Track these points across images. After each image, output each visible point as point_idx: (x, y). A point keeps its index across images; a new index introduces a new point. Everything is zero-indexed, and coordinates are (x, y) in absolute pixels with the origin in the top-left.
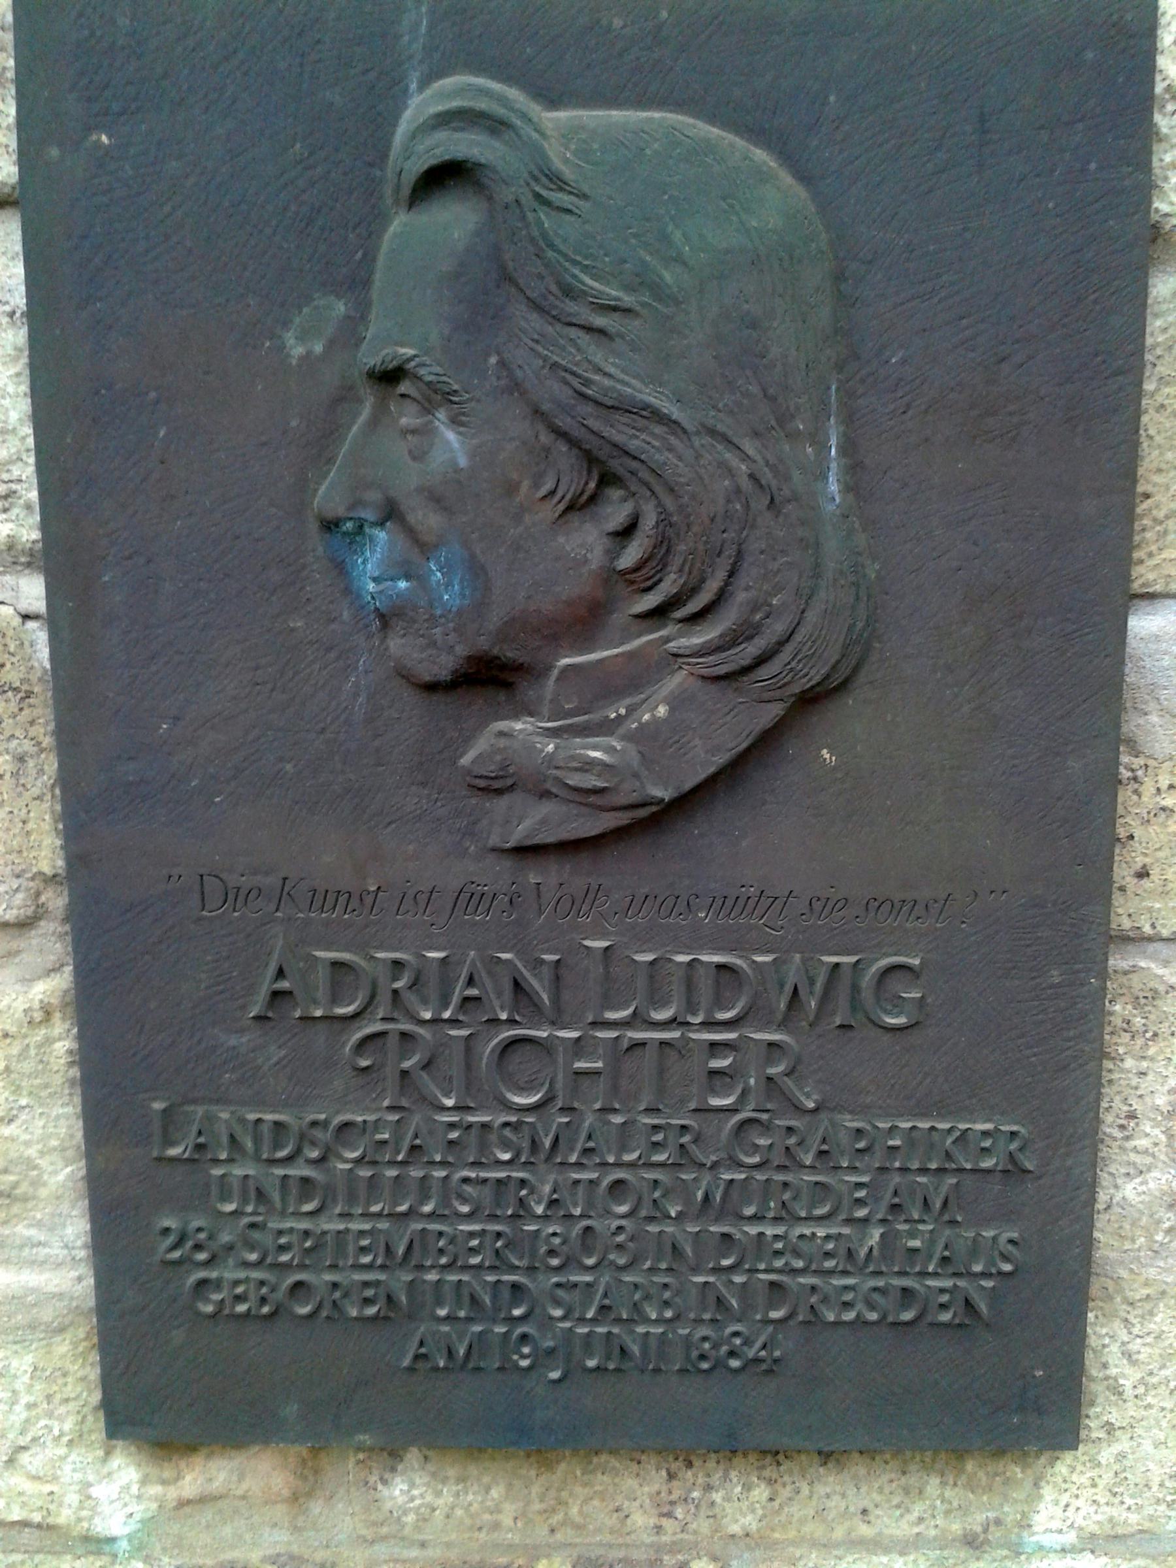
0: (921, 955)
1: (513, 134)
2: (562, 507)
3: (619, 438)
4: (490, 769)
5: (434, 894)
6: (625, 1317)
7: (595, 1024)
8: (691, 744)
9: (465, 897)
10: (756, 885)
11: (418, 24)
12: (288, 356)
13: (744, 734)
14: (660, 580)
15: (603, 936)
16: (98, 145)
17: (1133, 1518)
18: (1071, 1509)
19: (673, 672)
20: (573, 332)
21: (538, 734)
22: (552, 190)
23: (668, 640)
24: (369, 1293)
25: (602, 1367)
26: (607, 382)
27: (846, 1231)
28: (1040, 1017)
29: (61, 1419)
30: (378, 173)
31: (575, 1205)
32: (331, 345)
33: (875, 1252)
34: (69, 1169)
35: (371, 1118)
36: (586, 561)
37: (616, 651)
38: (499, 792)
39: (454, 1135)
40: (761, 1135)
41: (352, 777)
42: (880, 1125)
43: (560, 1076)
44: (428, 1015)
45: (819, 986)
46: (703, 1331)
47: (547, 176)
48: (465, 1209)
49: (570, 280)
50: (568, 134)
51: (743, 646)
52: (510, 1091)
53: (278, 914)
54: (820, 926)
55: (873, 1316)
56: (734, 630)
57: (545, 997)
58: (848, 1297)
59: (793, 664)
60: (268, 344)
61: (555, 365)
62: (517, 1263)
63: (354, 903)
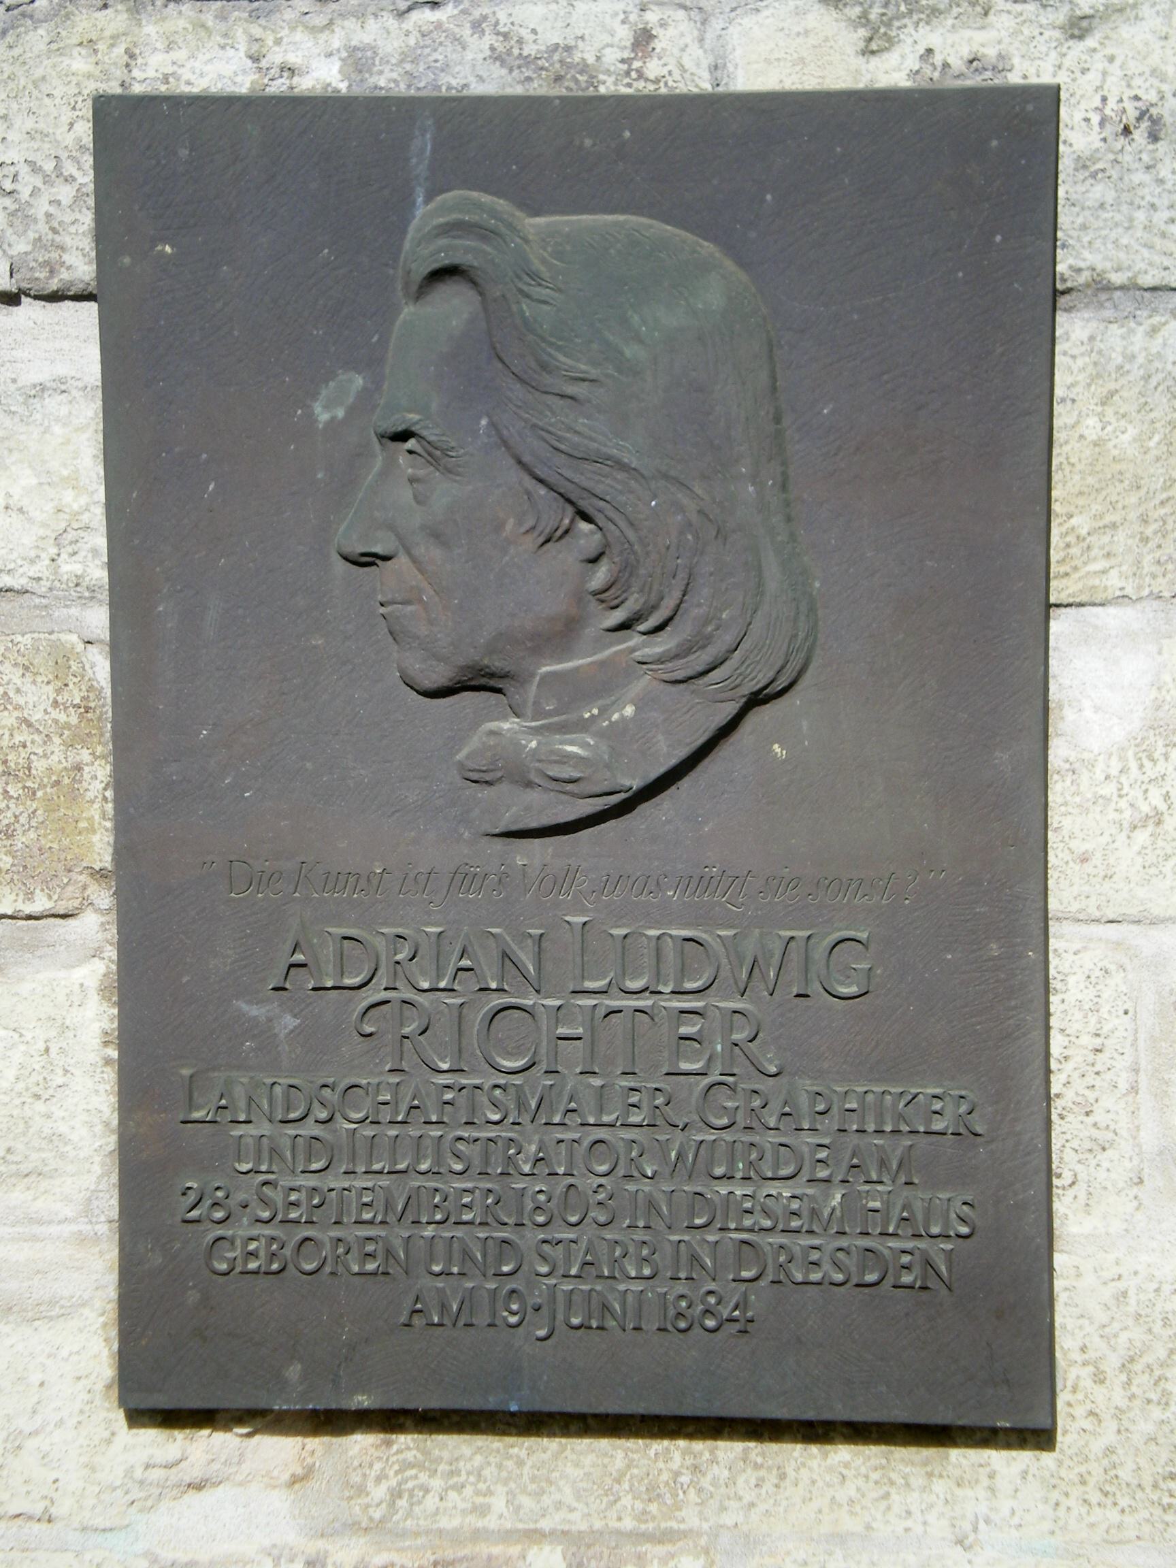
0: (869, 929)
1: (500, 240)
3: (585, 484)
4: (482, 764)
5: (432, 874)
6: (606, 1274)
8: (655, 740)
9: (459, 877)
10: (718, 865)
11: (423, 150)
12: (316, 421)
13: (701, 731)
15: (583, 912)
18: (1062, 1509)
19: (638, 678)
20: (550, 400)
21: (524, 732)
22: (530, 285)
24: (370, 1248)
25: (586, 1324)
26: (576, 439)
27: (810, 1191)
28: (983, 987)
31: (560, 1165)
32: (351, 411)
33: (838, 1213)
35: (375, 1081)
37: (589, 660)
39: (448, 1096)
40: (729, 1098)
41: (362, 772)
42: (838, 1089)
44: (426, 985)
46: (681, 1288)
47: (528, 274)
48: (458, 1167)
49: (546, 358)
51: (698, 654)
52: (499, 1055)
53: (297, 895)
54: (776, 903)
55: (839, 1277)
56: (690, 641)
57: (531, 968)
58: (815, 1256)
59: (743, 668)
60: (299, 412)
61: (534, 426)
62: (506, 1220)
63: (363, 883)
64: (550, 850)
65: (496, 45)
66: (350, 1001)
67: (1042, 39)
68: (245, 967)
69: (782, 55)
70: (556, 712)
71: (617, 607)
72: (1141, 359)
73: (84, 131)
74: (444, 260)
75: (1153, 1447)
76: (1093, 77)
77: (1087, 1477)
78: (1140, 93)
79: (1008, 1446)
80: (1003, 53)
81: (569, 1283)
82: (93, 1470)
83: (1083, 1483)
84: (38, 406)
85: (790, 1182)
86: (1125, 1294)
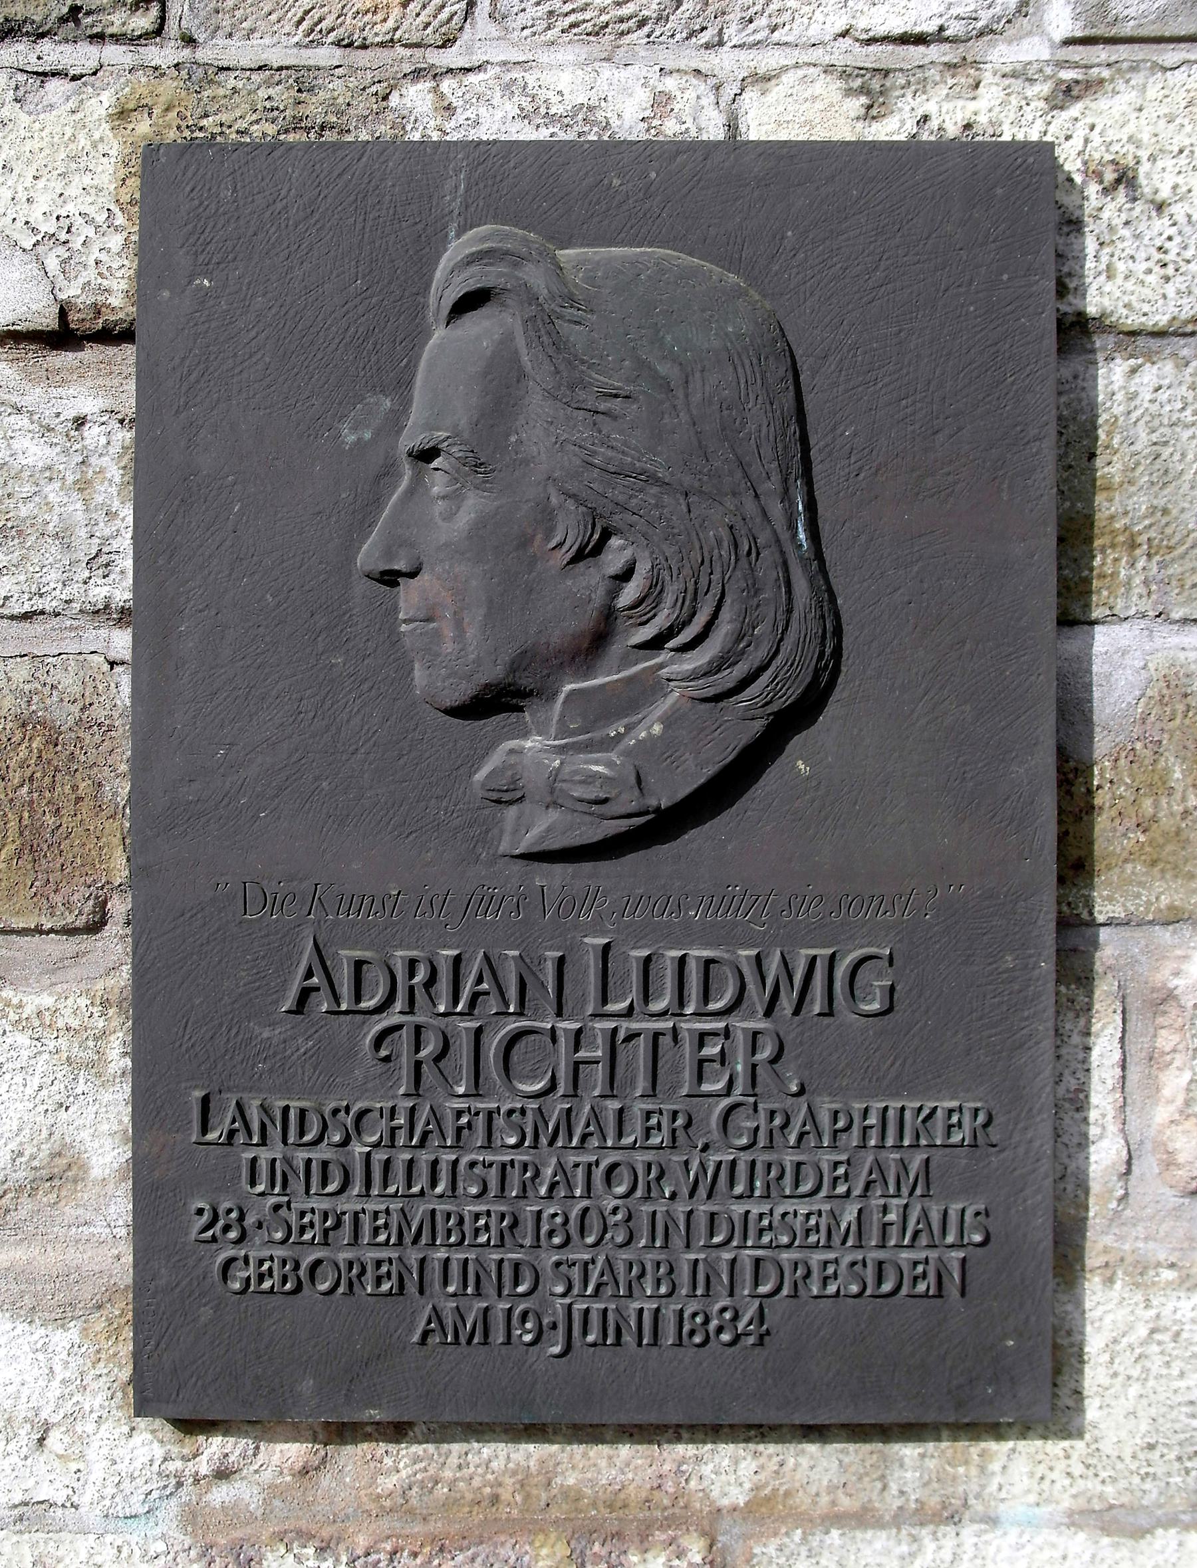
4: (503, 783)
7: (594, 1015)
14: (655, 615)
15: (603, 933)
16: (201, 287)
17: (1109, 1489)
18: (1047, 1482)
23: (661, 666)
29: (94, 1394)
30: (422, 300)
32: (377, 434)
37: (615, 677)
38: (510, 803)
43: (563, 1064)
50: (579, 264)
65: (524, 104)
67: (1028, 109)
68: (258, 988)
69: (791, 117)
74: (473, 285)
75: (1133, 1421)
80: (994, 120)
81: (583, 1302)
82: (114, 1463)
83: (1068, 1457)
84: (1071, 1050)
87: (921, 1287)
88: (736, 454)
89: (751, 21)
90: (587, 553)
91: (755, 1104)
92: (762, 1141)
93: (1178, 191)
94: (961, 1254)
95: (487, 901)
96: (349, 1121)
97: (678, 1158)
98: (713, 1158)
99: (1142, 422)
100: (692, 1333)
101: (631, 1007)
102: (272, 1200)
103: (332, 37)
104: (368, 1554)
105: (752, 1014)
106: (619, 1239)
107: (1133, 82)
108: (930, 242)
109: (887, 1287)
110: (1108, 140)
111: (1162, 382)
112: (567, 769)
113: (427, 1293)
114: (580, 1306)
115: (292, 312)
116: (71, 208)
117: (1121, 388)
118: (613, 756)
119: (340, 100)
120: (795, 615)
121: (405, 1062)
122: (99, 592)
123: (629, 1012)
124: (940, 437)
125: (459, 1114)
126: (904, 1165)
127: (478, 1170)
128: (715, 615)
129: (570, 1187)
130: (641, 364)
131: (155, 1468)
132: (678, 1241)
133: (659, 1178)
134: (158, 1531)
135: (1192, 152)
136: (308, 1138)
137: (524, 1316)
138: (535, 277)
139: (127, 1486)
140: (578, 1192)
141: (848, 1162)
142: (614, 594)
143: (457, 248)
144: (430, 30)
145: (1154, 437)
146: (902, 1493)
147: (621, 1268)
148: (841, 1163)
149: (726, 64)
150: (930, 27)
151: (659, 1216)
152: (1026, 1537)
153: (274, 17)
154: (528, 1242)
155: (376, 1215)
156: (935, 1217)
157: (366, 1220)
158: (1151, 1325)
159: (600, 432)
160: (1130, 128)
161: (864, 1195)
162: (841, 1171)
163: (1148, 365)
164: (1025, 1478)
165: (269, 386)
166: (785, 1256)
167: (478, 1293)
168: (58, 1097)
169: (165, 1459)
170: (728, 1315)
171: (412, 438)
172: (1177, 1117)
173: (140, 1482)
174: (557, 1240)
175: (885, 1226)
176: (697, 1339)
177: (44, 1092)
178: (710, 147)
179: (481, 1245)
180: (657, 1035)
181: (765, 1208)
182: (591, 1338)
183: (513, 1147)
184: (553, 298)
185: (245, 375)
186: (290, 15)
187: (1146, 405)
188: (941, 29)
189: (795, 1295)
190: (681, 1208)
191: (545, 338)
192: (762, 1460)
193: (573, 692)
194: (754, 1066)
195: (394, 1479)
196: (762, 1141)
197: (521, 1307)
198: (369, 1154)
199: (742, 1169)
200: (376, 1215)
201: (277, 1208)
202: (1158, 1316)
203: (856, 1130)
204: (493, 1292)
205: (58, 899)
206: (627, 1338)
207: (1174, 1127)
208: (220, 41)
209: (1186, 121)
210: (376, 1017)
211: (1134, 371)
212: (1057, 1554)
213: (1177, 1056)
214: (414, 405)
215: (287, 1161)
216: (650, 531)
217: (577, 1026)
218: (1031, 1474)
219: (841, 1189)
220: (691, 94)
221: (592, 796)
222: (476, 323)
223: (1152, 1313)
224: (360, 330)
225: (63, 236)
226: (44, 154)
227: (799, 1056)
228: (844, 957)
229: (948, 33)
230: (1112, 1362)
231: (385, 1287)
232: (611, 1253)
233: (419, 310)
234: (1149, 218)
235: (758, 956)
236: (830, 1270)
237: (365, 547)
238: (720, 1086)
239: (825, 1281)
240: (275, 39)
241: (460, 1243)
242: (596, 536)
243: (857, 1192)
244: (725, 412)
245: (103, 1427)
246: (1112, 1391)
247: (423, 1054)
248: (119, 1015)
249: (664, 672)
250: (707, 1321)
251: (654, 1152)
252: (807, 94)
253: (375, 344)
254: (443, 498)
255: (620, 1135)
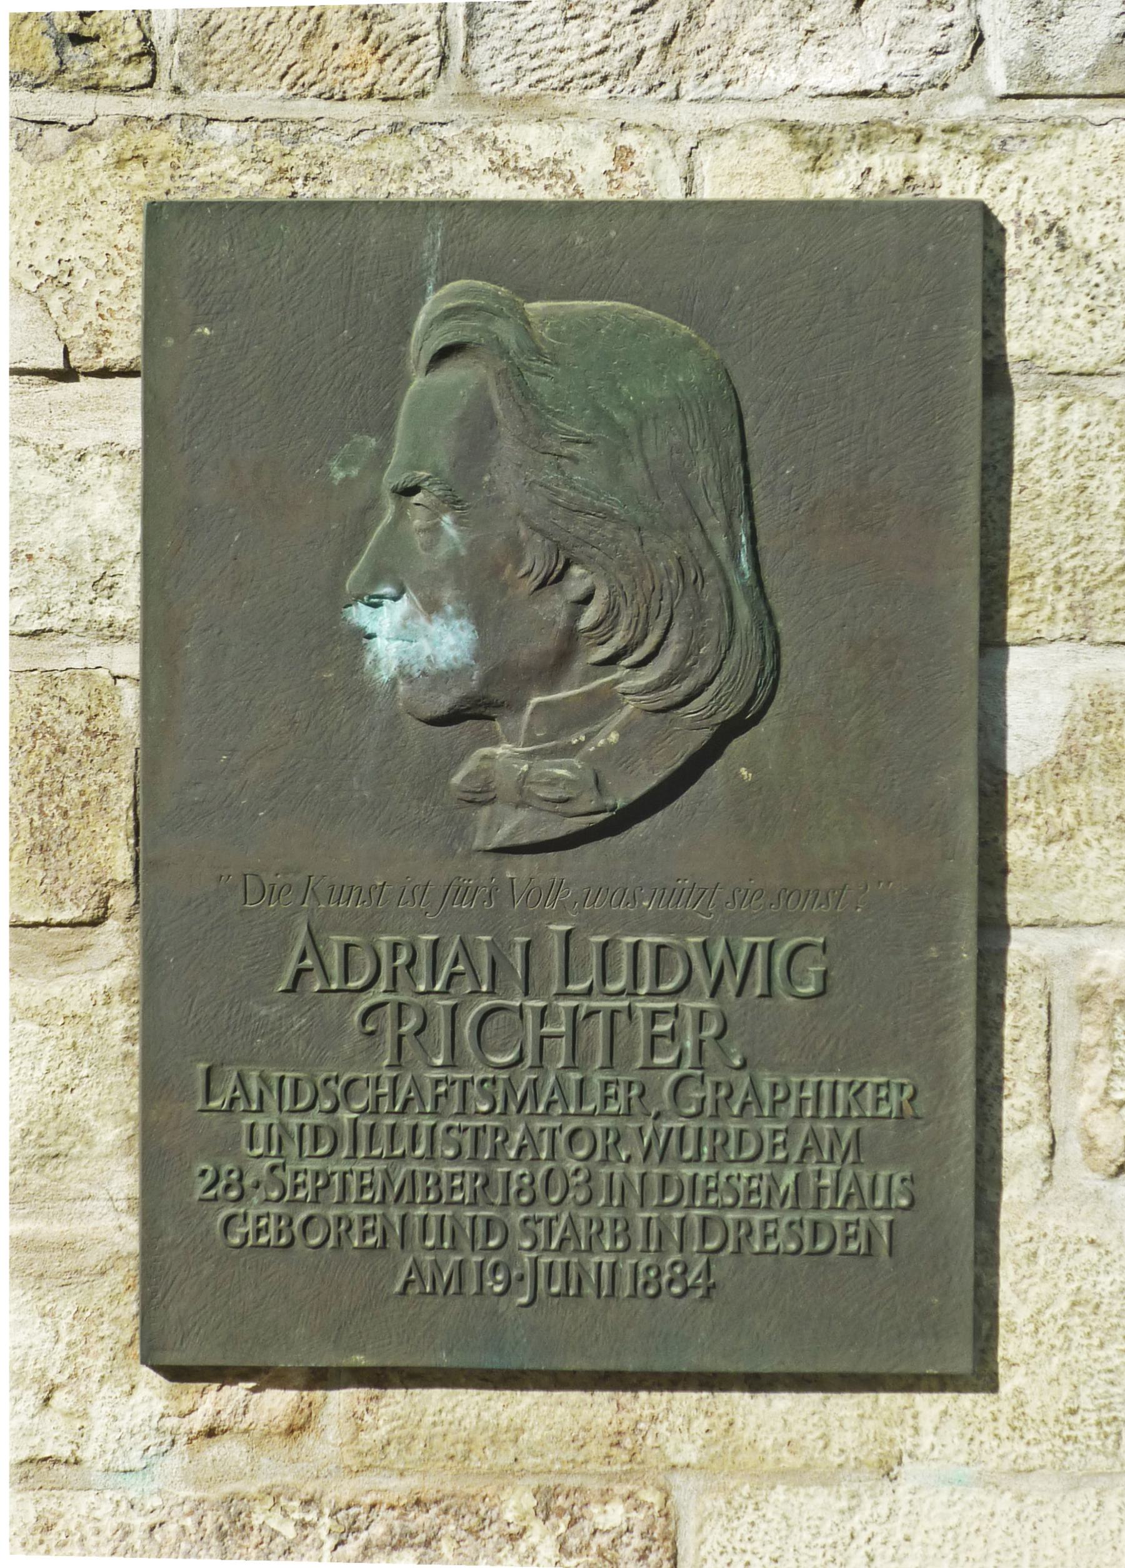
2: (536, 583)
4: (477, 784)
7: (558, 995)
11: (434, 245)
15: (565, 921)
16: (202, 336)
18: (976, 1442)
21: (515, 757)
23: (617, 682)
29: (97, 1356)
34: (117, 1131)
36: (554, 622)
37: (577, 691)
45: (741, 965)
50: (545, 317)
64: (536, 865)
66: (352, 1002)
70: (548, 739)
71: (603, 643)
72: (1051, 432)
73: (134, 235)
74: (451, 339)
76: (1011, 194)
77: (998, 1415)
78: (1049, 209)
79: (930, 1390)
82: (115, 1419)
83: (995, 1420)
85: (750, 1164)
86: (1035, 1254)
87: (853, 1247)
88: (684, 493)
89: (706, 76)
90: (554, 579)
91: (703, 1077)
92: (709, 1109)
93: (1106, 241)
94: (889, 1217)
95: (463, 892)
96: (339, 1090)
97: (633, 1125)
98: (665, 1126)
99: (1071, 458)
100: (646, 1285)
101: (591, 987)
102: (268, 1163)
103: (315, 90)
104: (349, 1507)
105: (699, 995)
106: (581, 1198)
107: (1064, 138)
108: (866, 295)
109: (822, 1246)
110: (1040, 192)
111: (1090, 419)
112: (534, 773)
113: (408, 1247)
114: (545, 1260)
115: (286, 359)
116: (71, 253)
117: (1051, 425)
118: (575, 762)
119: (323, 153)
120: (737, 636)
121: (389, 1036)
122: (104, 611)
123: (589, 992)
124: (873, 475)
125: (437, 1082)
126: (836, 1134)
127: (454, 1134)
128: (664, 637)
129: (537, 1150)
130: (599, 412)
131: (154, 1424)
132: (634, 1202)
133: (616, 1143)
134: (154, 1486)
135: (1119, 204)
136: (301, 1105)
137: (495, 1268)
138: (505, 331)
139: (127, 1442)
140: (544, 1155)
141: (787, 1131)
142: (575, 617)
143: (433, 303)
144: (405, 85)
145: (1082, 471)
146: (842, 1451)
147: (582, 1225)
148: (780, 1131)
149: (684, 119)
150: (875, 85)
151: (616, 1178)
152: (956, 1496)
153: (258, 71)
154: (499, 1200)
155: (362, 1175)
156: (866, 1182)
157: (353, 1180)
158: (1073, 1298)
159: (563, 474)
160: (1062, 181)
161: (800, 1162)
162: (780, 1139)
163: (1078, 403)
164: (956, 1440)
165: (265, 427)
166: (730, 1216)
167: (454, 1248)
168: (64, 1080)
169: (163, 1416)
170: (678, 1269)
171: (393, 477)
172: (1098, 1105)
173: (138, 1438)
174: (525, 1199)
175: (820, 1189)
176: (651, 1291)
177: (51, 1076)
178: (665, 208)
179: (456, 1203)
180: (614, 1012)
181: (712, 1171)
182: (555, 1289)
183: (485, 1113)
184: (522, 352)
185: (244, 415)
186: (274, 68)
187: (1076, 440)
188: (885, 86)
189: (738, 1251)
190: (635, 1171)
191: (515, 390)
192: (714, 1419)
193: (538, 705)
194: (701, 1042)
195: (375, 1435)
196: (709, 1109)
197: (493, 1260)
198: (356, 1120)
199: (691, 1135)
200: (362, 1175)
201: (273, 1168)
202: (1079, 1289)
203: (793, 1102)
204: (467, 1246)
205: (65, 895)
206: (589, 1290)
207: (1095, 1114)
208: (208, 93)
209: (1114, 175)
210: (363, 996)
211: (1064, 409)
212: (986, 1511)
213: (1100, 1050)
214: (397, 444)
215: (283, 1126)
216: (608, 562)
217: (542, 1004)
218: (962, 1435)
219: (780, 1155)
220: (649, 149)
221: (556, 796)
222: (452, 373)
223: (1074, 1286)
224: (348, 376)
225: (65, 279)
226: (45, 200)
227: (742, 1034)
228: (783, 944)
229: (891, 90)
230: (1037, 1331)
231: (370, 1241)
232: (573, 1212)
233: (399, 359)
234: (1078, 266)
235: (704, 943)
236: (771, 1229)
237: (353, 573)
238: (670, 1060)
239: (765, 1239)
240: (260, 93)
241: (438, 1200)
242: (560, 566)
243: (795, 1158)
244: (675, 456)
245: (106, 1387)
246: (1037, 1359)
247: (404, 1029)
248: (122, 1002)
249: (620, 687)
250: (659, 1274)
251: (612, 1119)
252: (759, 148)
253: (361, 388)
254: (424, 531)
255: (581, 1103)
